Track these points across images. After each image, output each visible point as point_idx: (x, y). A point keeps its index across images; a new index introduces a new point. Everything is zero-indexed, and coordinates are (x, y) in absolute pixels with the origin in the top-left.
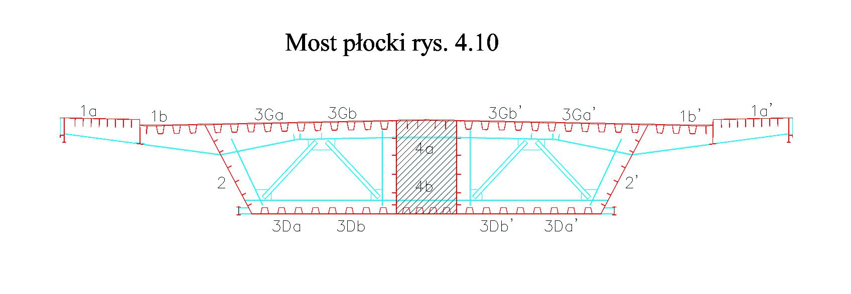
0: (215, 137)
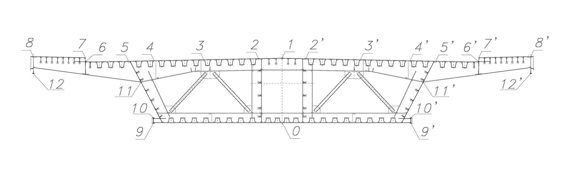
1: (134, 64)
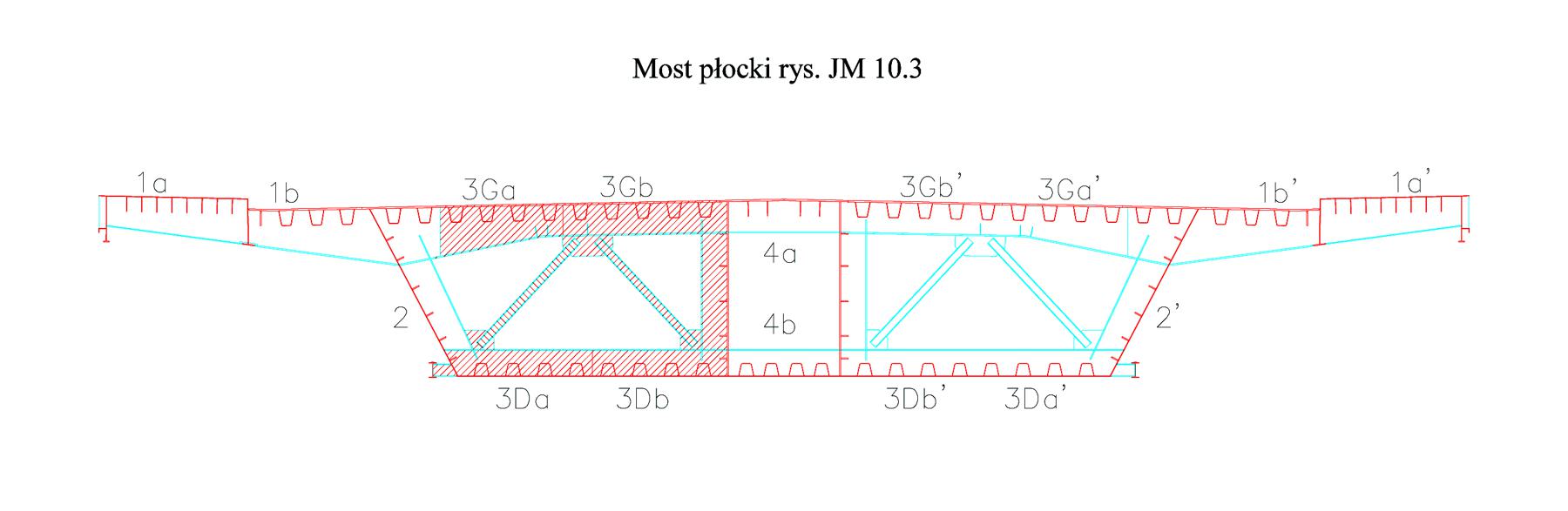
0: (389, 231)
1: (380, 214)
